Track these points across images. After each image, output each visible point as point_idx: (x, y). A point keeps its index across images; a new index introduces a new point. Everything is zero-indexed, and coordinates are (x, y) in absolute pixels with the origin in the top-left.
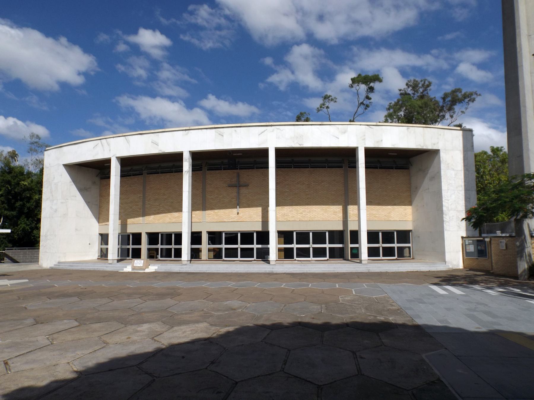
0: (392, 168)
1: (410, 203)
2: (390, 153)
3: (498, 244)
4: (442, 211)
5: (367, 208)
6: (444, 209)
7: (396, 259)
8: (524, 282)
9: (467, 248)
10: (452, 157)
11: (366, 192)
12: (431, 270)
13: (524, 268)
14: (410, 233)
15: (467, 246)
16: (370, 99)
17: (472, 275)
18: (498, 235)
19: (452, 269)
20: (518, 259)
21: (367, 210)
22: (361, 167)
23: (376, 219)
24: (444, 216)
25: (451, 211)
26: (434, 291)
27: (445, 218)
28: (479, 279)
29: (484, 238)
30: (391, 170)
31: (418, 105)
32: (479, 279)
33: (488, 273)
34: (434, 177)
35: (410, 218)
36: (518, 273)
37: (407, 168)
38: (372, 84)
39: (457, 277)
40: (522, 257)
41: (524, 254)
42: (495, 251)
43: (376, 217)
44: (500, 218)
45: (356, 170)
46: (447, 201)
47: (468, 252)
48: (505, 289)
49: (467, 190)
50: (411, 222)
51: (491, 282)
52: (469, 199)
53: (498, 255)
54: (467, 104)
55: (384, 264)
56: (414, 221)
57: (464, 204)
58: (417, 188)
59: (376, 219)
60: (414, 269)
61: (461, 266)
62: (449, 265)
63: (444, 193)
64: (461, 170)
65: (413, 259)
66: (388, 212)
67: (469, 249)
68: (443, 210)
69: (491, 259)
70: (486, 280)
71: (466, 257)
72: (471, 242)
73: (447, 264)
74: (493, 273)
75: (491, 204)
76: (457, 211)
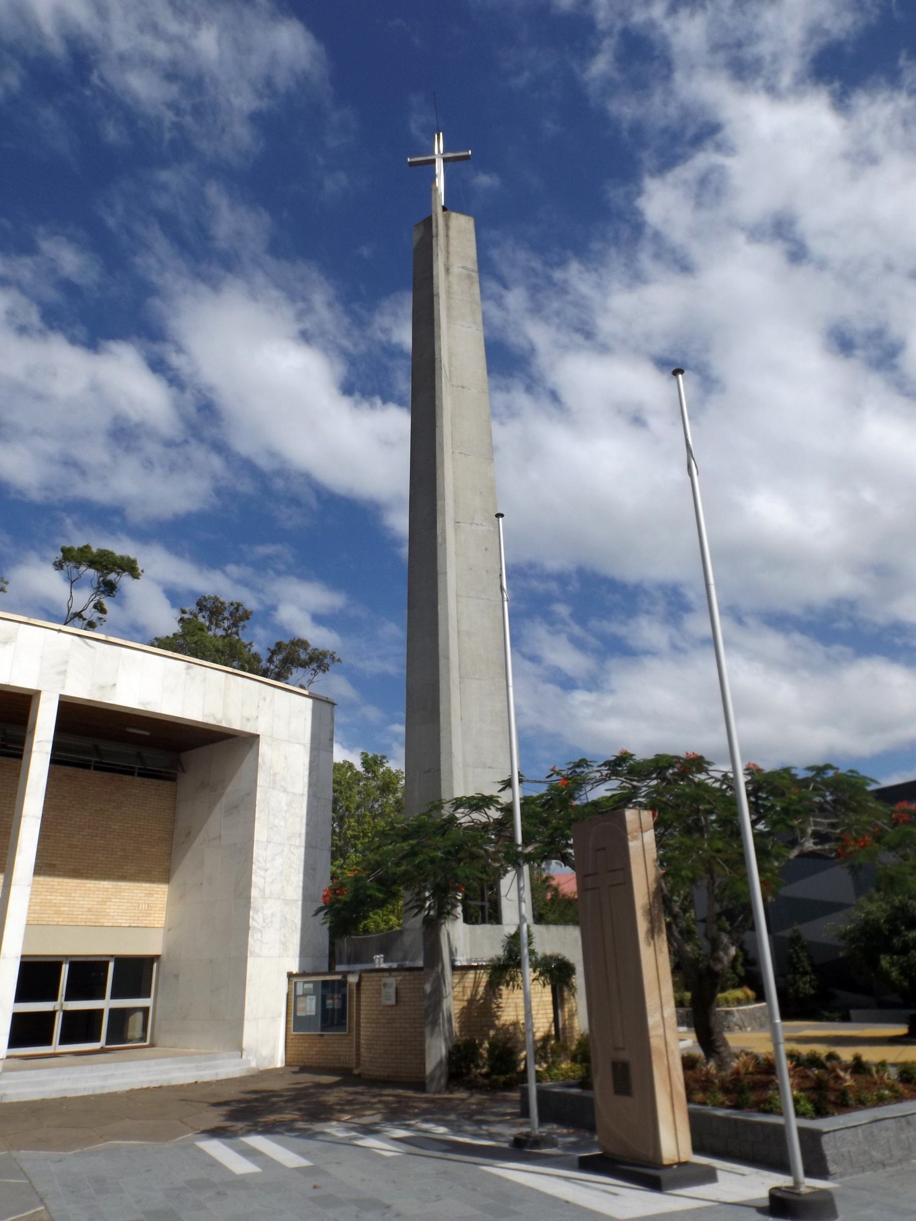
0: (129, 772)
1: (165, 877)
2: (130, 727)
3: (379, 992)
4: (248, 898)
5: (34, 883)
6: (254, 893)
7: (102, 1051)
8: (443, 1099)
9: (300, 1006)
10: (286, 757)
11: (40, 835)
12: (199, 1081)
13: (438, 1058)
14: (155, 965)
15: (298, 999)
16: (103, 611)
17: (307, 1088)
18: (377, 966)
19: (258, 1069)
20: (427, 1030)
21: (34, 893)
22: (40, 752)
23: (60, 920)
24: (251, 913)
25: (269, 900)
26: (214, 1164)
27: (253, 919)
28: (332, 1097)
29: (345, 974)
30: (127, 778)
31: (214, 646)
32: (332, 1097)
33: (348, 1076)
34: (236, 807)
35: (159, 918)
36: (424, 1072)
37: (171, 777)
38: (112, 576)
39: (275, 1099)
40: (435, 1023)
41: (441, 1015)
42: (370, 1012)
43: (58, 913)
44: (372, 924)
45: (21, 764)
46: (262, 873)
47: (301, 1017)
48: (408, 1127)
49: (310, 847)
50: (162, 931)
51: (366, 1106)
52: (314, 869)
53: (376, 1023)
54: (313, 672)
55: (58, 1069)
56: (168, 929)
57: (301, 884)
58: (190, 835)
59: (59, 920)
60: (151, 1081)
61: (279, 1062)
62: (250, 1058)
63: (259, 852)
64: (303, 795)
65: (152, 1045)
66: (100, 900)
67: (304, 1009)
68: (250, 897)
69: (358, 1034)
70: (350, 1103)
71: (294, 1031)
72: (310, 989)
73: (244, 1057)
74: (359, 1076)
75: (398, 864)
76: (284, 900)
